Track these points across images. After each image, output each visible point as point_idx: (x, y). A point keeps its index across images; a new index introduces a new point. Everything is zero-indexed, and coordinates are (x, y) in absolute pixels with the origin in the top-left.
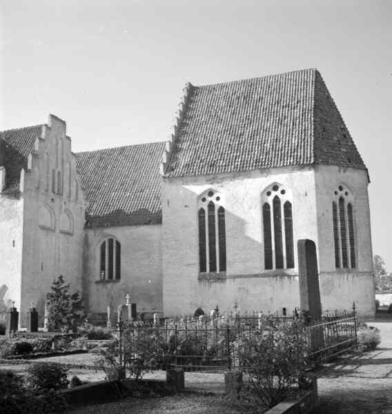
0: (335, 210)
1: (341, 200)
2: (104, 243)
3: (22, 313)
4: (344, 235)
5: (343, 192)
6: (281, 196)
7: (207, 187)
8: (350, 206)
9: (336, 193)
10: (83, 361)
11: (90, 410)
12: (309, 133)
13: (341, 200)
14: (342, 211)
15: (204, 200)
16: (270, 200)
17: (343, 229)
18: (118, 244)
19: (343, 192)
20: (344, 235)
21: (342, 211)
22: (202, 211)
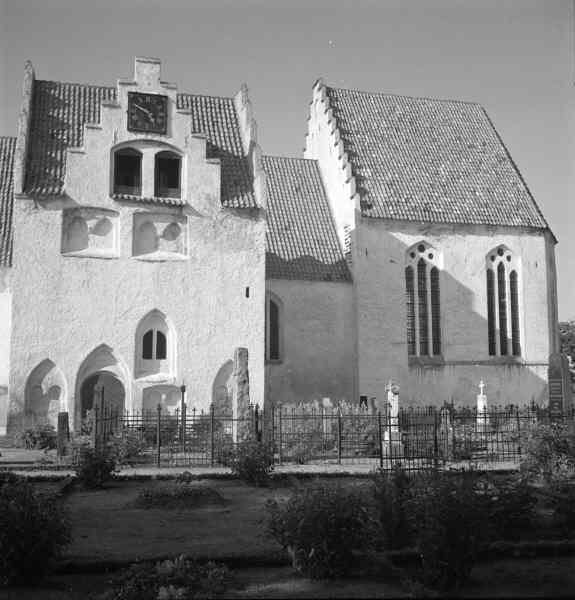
13: (501, 268)
21: (422, 278)
22: (409, 271)
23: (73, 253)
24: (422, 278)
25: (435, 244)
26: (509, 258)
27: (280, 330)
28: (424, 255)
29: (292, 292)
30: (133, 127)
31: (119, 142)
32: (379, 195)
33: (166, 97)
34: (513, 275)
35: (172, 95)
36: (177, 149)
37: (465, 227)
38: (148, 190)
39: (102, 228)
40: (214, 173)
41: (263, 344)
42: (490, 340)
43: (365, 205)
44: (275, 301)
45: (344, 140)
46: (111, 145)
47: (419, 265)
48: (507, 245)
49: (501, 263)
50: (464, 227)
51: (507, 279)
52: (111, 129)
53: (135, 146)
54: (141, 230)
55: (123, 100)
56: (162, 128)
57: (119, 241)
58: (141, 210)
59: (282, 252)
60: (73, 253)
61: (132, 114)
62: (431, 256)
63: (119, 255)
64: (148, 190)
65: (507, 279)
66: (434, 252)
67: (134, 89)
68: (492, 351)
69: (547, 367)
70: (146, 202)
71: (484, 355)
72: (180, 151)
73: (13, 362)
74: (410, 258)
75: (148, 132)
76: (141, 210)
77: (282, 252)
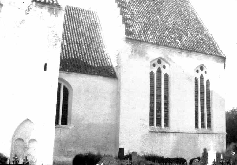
4: (159, 116)
13: (159, 71)
15: (154, 65)
20: (159, 116)
21: (159, 80)
22: (152, 74)
24: (159, 80)
26: (206, 72)
27: (69, 108)
28: (161, 66)
29: (77, 81)
42: (58, 92)
44: (67, 86)
45: (126, 24)
47: (200, 78)
49: (202, 75)
59: (90, 61)
66: (166, 65)
68: (196, 126)
69: (226, 135)
71: (192, 128)
77: (90, 61)
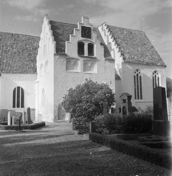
0: (135, 79)
1: (137, 75)
2: (16, 88)
3: (167, 88)
5: (138, 72)
6: (139, 74)
7: (154, 70)
8: (140, 77)
9: (135, 72)
10: (50, 134)
11: (79, 149)
12: (15, 47)
13: (137, 75)
14: (137, 79)
16: (136, 75)
17: (138, 86)
18: (22, 90)
19: (138, 72)
21: (137, 79)
22: (135, 76)
23: (71, 71)
25: (141, 70)
30: (83, 36)
31: (79, 40)
32: (127, 56)
33: (90, 28)
34: (158, 78)
35: (92, 28)
36: (93, 42)
37: (109, 60)
38: (86, 53)
39: (75, 64)
40: (102, 49)
41: (143, 94)
43: (124, 59)
46: (77, 41)
48: (157, 70)
49: (137, 74)
50: (148, 64)
51: (157, 79)
52: (77, 37)
53: (83, 41)
54: (68, 62)
55: (79, 28)
56: (89, 36)
57: (80, 68)
58: (86, 59)
60: (71, 71)
61: (83, 32)
62: (139, 73)
63: (80, 72)
64: (86, 53)
65: (157, 79)
67: (83, 25)
70: (86, 57)
72: (94, 43)
73: (54, 101)
74: (135, 73)
75: (87, 37)
76: (86, 59)
